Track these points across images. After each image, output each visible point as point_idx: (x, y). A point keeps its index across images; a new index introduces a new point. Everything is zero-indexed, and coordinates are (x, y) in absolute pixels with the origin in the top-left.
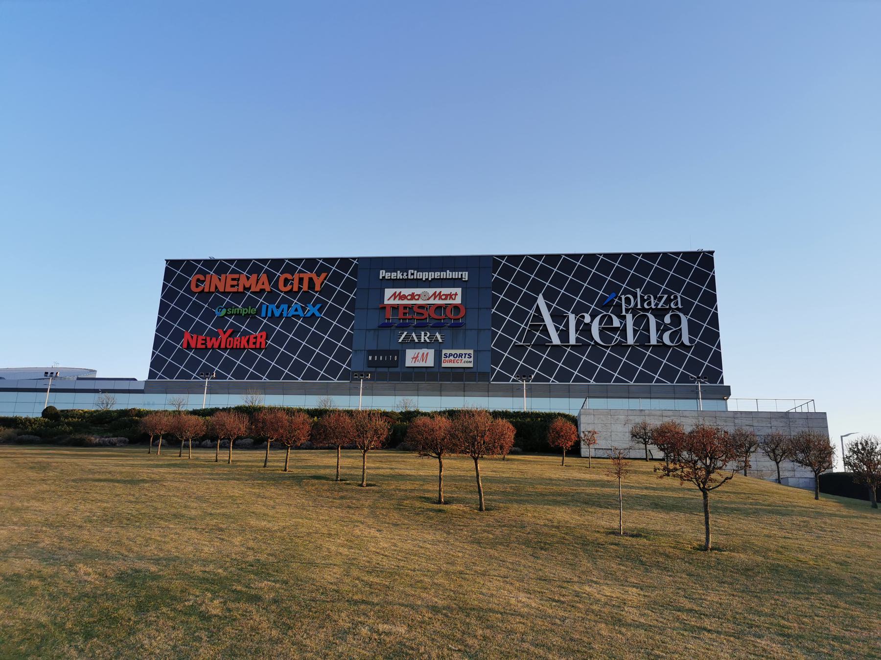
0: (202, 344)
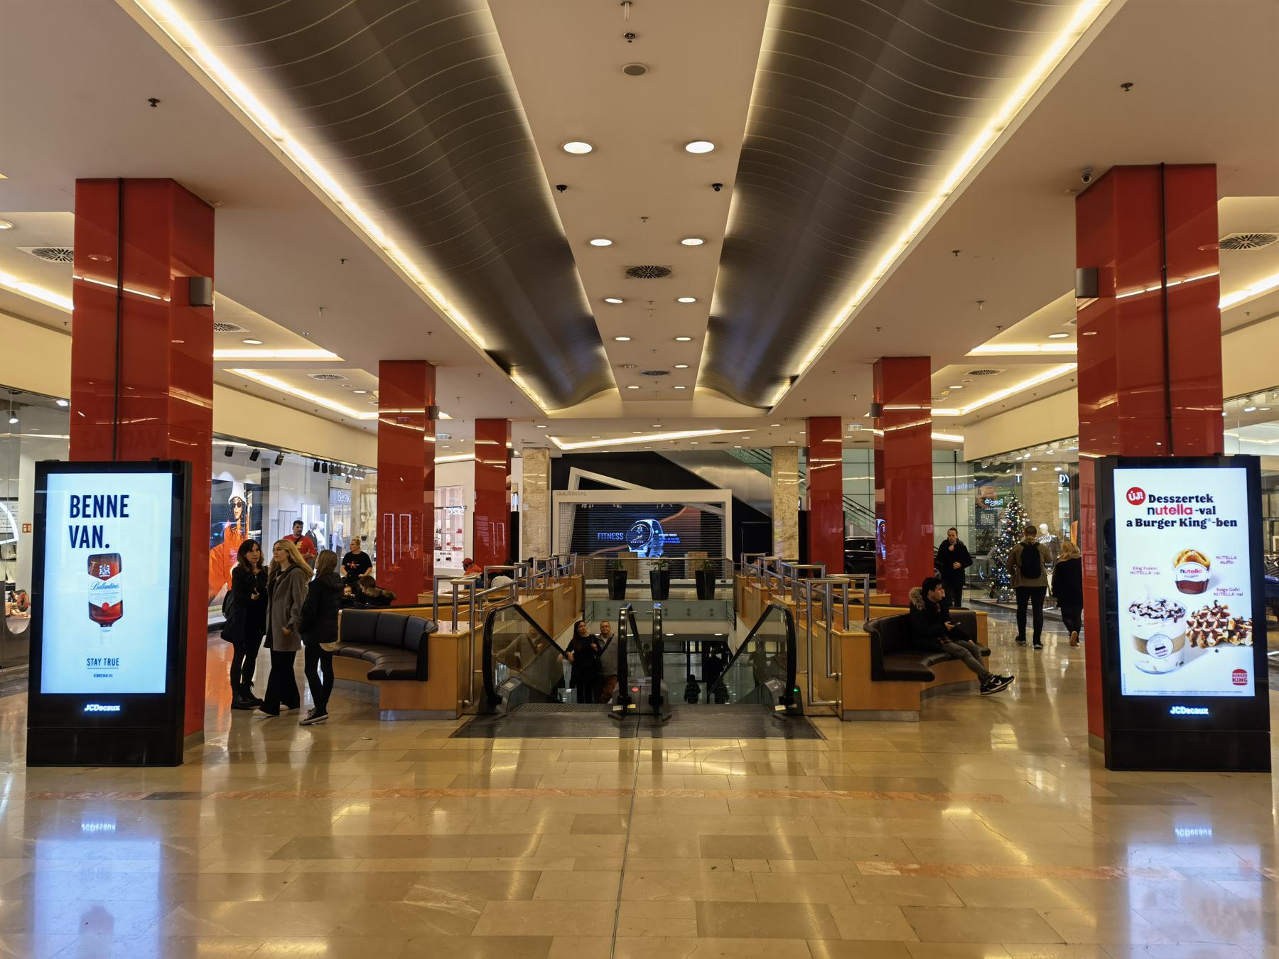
0: (114, 506)
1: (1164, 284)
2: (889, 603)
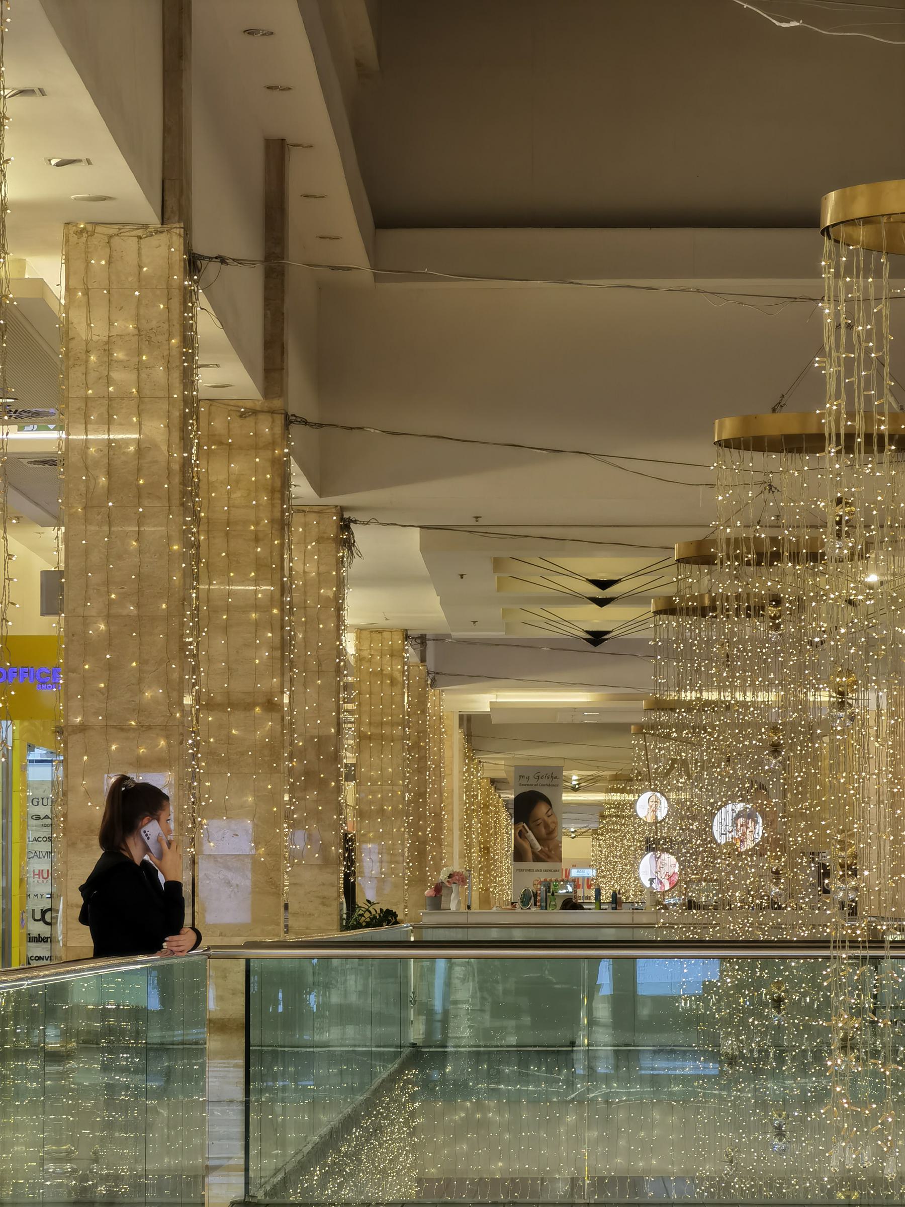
2: (92, 956)
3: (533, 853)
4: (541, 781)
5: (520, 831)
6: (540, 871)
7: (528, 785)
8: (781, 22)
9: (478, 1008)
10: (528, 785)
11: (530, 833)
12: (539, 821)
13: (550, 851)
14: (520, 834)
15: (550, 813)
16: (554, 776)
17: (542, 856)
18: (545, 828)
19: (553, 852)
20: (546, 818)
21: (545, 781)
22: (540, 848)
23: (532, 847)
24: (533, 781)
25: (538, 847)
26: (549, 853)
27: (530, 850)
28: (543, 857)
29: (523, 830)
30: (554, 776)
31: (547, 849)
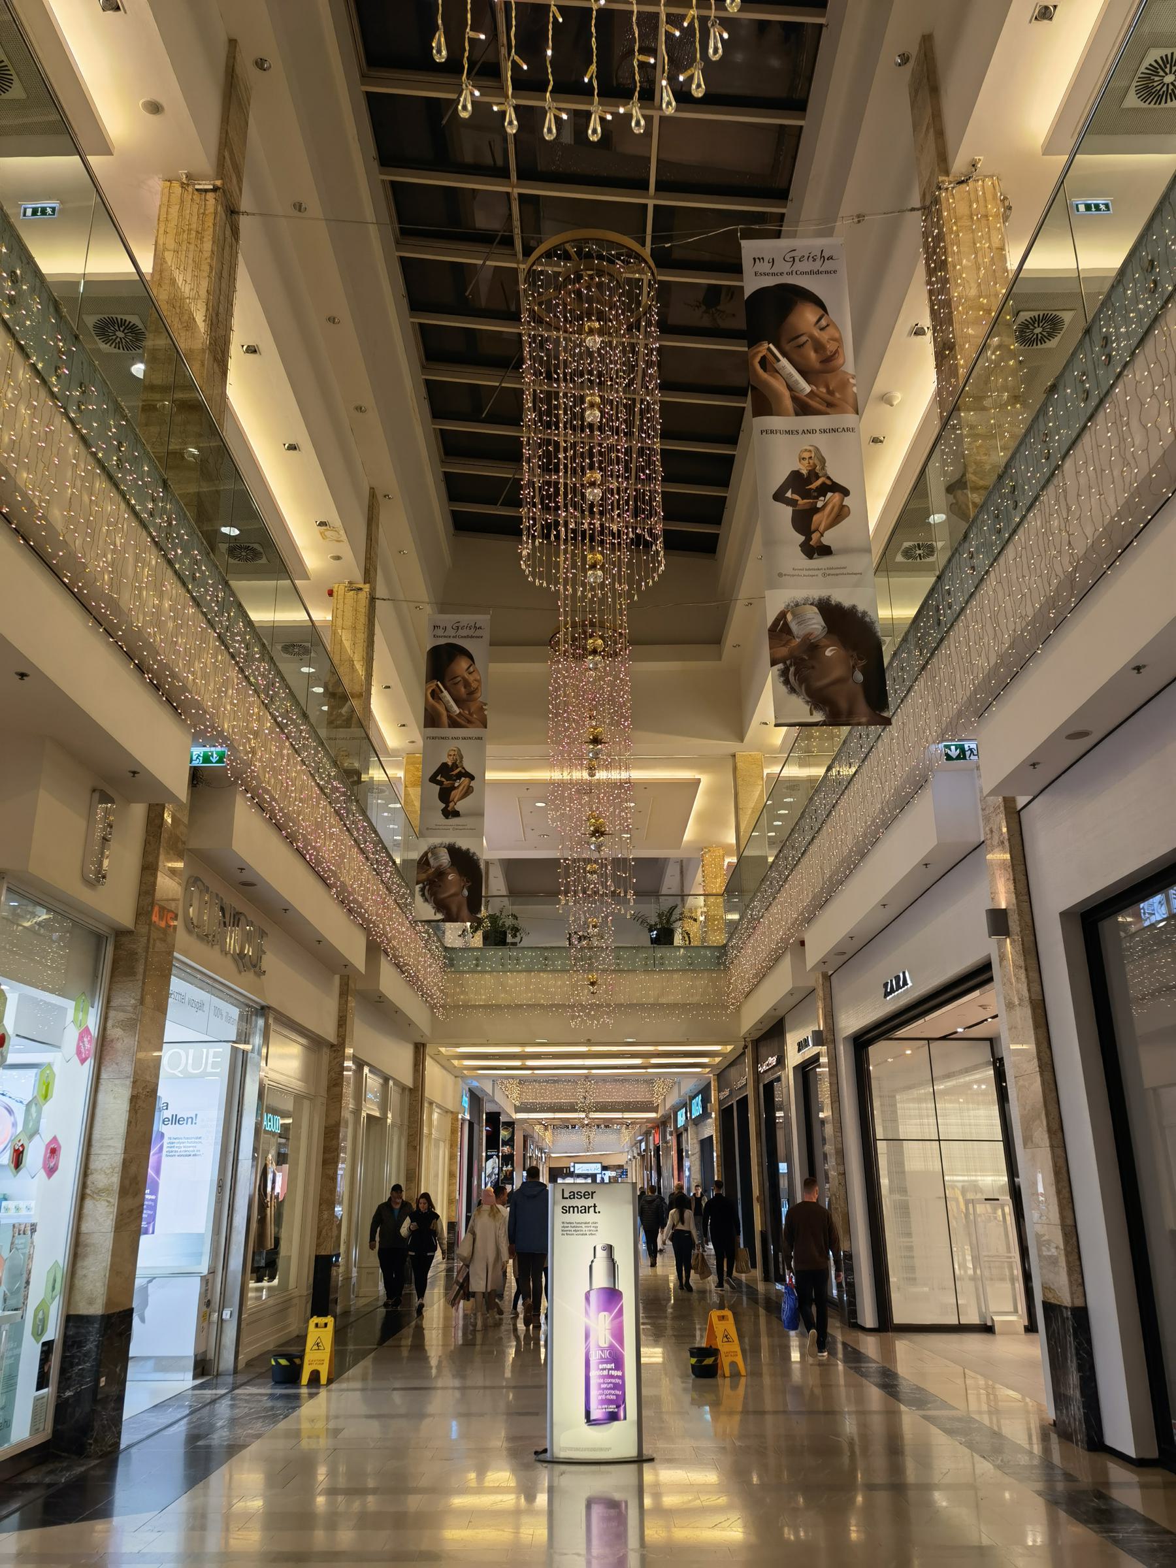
1: (484, 263)
3: (449, 717)
4: (799, 266)
5: (433, 691)
6: (813, 432)
7: (774, 274)
8: (638, 24)
9: (970, 476)
10: (774, 274)
11: (446, 693)
12: (804, 339)
13: (830, 392)
14: (435, 694)
15: (471, 669)
16: (477, 626)
17: (814, 404)
18: (816, 351)
19: (837, 395)
20: (816, 333)
21: (806, 266)
22: (458, 711)
23: (447, 710)
24: (452, 633)
25: (456, 710)
26: (828, 397)
27: (444, 713)
28: (463, 722)
29: (770, 356)
30: (477, 626)
31: (824, 390)
